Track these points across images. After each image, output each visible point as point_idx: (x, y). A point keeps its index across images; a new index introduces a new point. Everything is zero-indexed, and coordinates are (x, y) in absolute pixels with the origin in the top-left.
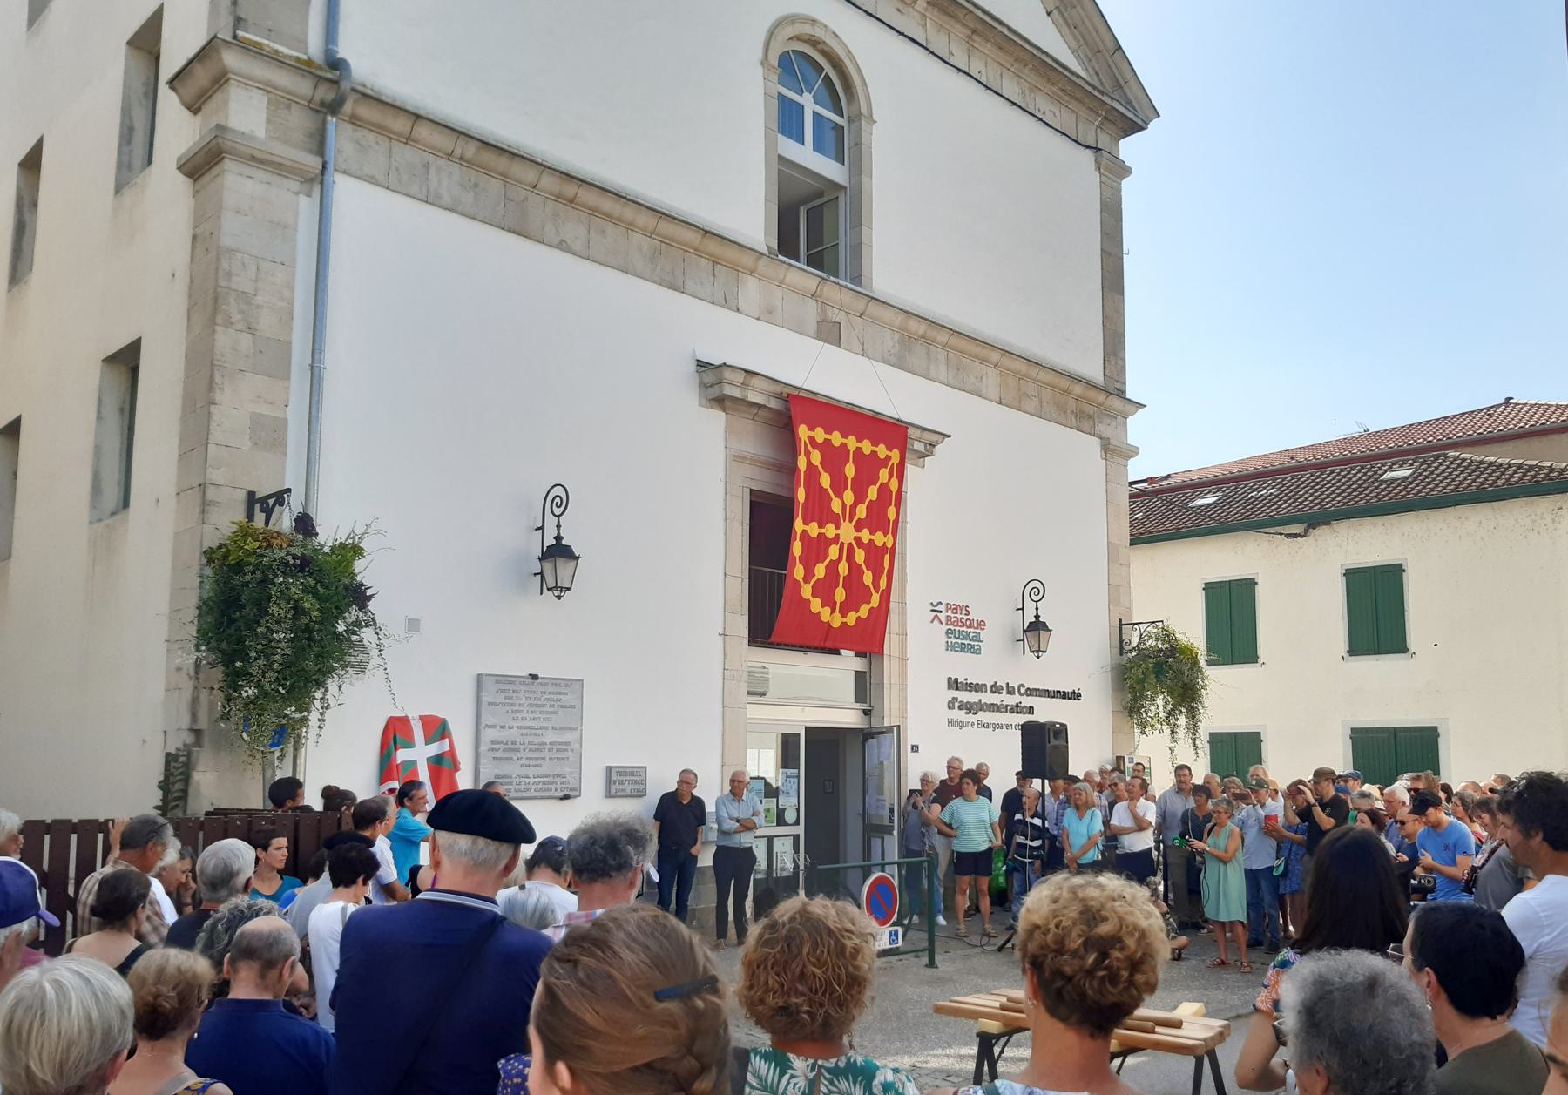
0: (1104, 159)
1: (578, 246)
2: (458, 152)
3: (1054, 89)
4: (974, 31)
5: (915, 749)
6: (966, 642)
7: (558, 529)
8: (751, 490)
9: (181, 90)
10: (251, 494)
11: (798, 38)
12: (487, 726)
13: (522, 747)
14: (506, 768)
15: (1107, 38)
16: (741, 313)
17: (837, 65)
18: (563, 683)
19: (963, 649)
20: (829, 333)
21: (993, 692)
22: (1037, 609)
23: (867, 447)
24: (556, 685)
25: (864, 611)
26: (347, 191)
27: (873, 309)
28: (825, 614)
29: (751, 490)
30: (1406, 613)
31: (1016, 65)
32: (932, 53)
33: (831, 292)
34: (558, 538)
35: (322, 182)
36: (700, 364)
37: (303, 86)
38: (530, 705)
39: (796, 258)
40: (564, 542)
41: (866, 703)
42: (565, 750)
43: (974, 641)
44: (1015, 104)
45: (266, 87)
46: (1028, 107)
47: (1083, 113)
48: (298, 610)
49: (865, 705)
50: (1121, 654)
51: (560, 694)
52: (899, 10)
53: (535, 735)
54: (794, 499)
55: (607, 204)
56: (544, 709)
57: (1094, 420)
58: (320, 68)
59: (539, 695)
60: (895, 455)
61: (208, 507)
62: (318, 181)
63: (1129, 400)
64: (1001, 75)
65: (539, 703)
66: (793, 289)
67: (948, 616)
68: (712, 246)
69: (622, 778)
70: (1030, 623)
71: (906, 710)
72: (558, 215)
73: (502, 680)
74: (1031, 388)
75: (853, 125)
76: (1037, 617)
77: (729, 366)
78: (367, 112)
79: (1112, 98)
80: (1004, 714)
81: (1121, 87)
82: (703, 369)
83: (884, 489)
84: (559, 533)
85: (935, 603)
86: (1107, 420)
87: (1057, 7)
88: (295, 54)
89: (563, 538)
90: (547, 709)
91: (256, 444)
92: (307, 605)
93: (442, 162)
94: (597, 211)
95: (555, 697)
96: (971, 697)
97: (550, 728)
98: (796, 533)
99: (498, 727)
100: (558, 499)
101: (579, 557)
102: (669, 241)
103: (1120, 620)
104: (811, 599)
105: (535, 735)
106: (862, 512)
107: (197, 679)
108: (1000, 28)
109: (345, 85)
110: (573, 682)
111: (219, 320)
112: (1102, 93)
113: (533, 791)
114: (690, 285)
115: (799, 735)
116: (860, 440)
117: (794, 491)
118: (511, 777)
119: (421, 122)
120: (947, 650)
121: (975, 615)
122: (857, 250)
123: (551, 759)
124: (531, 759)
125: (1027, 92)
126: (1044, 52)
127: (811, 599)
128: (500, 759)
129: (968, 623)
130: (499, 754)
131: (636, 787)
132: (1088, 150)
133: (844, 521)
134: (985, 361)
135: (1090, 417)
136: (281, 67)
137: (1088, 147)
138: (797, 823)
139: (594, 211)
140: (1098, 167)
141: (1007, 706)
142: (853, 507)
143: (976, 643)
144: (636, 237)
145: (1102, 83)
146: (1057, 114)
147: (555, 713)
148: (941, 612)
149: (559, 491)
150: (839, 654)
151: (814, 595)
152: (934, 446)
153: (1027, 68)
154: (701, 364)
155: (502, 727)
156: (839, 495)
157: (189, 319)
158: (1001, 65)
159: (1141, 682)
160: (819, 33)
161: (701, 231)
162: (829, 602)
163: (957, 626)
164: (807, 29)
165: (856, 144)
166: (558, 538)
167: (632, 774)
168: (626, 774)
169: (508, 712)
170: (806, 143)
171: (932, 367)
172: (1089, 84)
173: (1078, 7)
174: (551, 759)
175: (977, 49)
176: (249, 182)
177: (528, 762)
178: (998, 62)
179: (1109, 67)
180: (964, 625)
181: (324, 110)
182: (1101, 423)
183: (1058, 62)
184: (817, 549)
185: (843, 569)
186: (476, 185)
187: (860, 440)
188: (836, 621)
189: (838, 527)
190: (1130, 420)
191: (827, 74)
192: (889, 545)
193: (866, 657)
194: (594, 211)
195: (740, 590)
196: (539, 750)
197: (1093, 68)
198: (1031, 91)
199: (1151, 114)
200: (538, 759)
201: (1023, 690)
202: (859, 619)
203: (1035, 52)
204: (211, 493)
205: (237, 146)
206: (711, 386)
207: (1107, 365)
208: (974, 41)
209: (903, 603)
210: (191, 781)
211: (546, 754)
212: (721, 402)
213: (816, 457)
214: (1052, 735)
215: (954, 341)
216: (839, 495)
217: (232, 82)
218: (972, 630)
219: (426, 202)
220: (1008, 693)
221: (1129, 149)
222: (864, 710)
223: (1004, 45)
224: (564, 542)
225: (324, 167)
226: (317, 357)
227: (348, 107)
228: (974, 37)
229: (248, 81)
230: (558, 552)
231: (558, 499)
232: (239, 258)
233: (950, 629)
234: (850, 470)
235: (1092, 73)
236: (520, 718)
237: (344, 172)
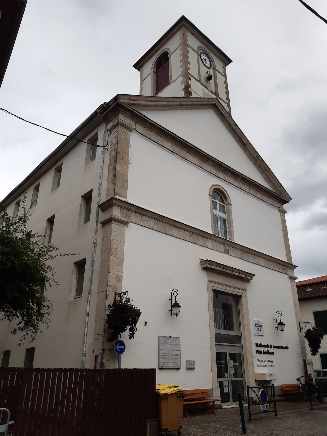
10: (116, 293)
34: (176, 302)
44: (260, 199)
46: (274, 205)
52: (234, 181)
73: (163, 337)
76: (281, 321)
82: (201, 261)
84: (176, 301)
87: (267, 178)
89: (177, 302)
95: (175, 342)
100: (175, 292)
103: (299, 322)
107: (104, 337)
115: (226, 353)
124: (170, 358)
130: (164, 357)
137: (277, 207)
138: (228, 377)
145: (278, 193)
146: (269, 200)
157: (102, 254)
166: (176, 302)
174: (174, 358)
182: (288, 271)
197: (276, 190)
204: (108, 293)
231: (175, 292)
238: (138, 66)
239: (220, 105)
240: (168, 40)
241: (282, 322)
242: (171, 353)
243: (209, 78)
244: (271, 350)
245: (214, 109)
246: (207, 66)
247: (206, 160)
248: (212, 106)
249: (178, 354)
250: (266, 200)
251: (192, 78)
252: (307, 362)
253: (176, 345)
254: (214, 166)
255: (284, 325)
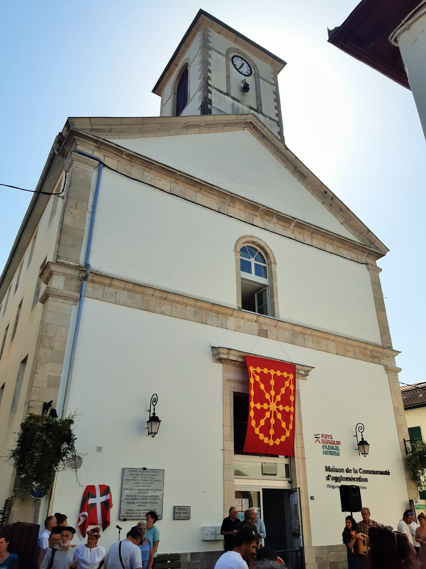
0: (370, 267)
1: (167, 313)
2: (127, 287)
3: (346, 246)
4: (312, 232)
5: (312, 498)
6: (332, 451)
7: (154, 411)
8: (234, 392)
9: (43, 278)
11: (248, 242)
12: (125, 489)
13: (138, 498)
14: (132, 507)
15: (364, 228)
16: (228, 329)
17: (262, 248)
18: (156, 471)
19: (331, 453)
20: (263, 333)
21: (347, 472)
22: (362, 435)
23: (279, 373)
24: (153, 472)
25: (283, 438)
26: (88, 303)
27: (279, 324)
28: (266, 440)
29: (234, 392)
30: (418, 408)
31: (330, 241)
32: (297, 241)
33: (263, 319)
35: (80, 300)
36: (213, 348)
37: (76, 273)
38: (143, 480)
39: (254, 311)
40: (156, 415)
41: (289, 478)
42: (157, 499)
43: (336, 450)
44: (331, 253)
45: (64, 274)
47: (359, 253)
48: (45, 445)
49: (289, 479)
50: (407, 454)
51: (155, 475)
52: (284, 230)
53: (144, 492)
54: (249, 394)
55: (178, 298)
56: (148, 482)
57: (379, 358)
58: (83, 267)
59: (146, 476)
60: (291, 376)
61: (30, 409)
62: (79, 300)
63: (394, 350)
64: (325, 244)
65: (146, 479)
66: (248, 320)
67: (323, 440)
68: (216, 308)
69: (180, 511)
70: (360, 441)
71: (307, 481)
72: (161, 303)
74: (350, 348)
75: (269, 266)
76: (363, 439)
77: (221, 347)
78: (96, 278)
79: (369, 247)
80: (353, 482)
81: (373, 243)
82: (213, 349)
83: (288, 389)
84: (154, 412)
85: (316, 434)
86: (385, 358)
88: (75, 264)
90: (149, 482)
91: (49, 386)
92: (48, 443)
93: (121, 291)
94: (174, 301)
95: (153, 477)
96: (338, 475)
97: (150, 490)
98: (251, 408)
99: (129, 489)
101: (161, 421)
102: (201, 308)
103: (404, 439)
104: (259, 434)
105: (144, 492)
106: (279, 398)
108: (322, 230)
109: (88, 271)
110: (161, 471)
111: (41, 346)
112: (365, 246)
113: (142, 516)
114: (208, 322)
116: (275, 371)
117: (249, 390)
118: (133, 510)
119: (113, 279)
120: (324, 454)
121: (335, 439)
122: (273, 304)
123: (150, 503)
124: (142, 503)
125: (336, 249)
126: (340, 236)
127: (259, 434)
128: (130, 503)
129: (332, 442)
131: (186, 515)
132: (363, 264)
133: (271, 402)
134: (328, 339)
135: (377, 357)
136: (69, 269)
139: (173, 301)
140: (368, 269)
141: (355, 478)
142: (275, 397)
143: (337, 451)
144: (189, 308)
145: (365, 243)
146: (349, 254)
147: (153, 483)
148: (319, 438)
149: (155, 396)
150: (278, 457)
151: (260, 432)
152: (308, 372)
153: (335, 241)
154: (213, 348)
155: (131, 489)
156: (269, 392)
158: (324, 241)
159: (415, 466)
160: (255, 240)
161: (212, 304)
162: (267, 435)
163: (327, 443)
164: (251, 239)
165: (271, 272)
166: (154, 414)
167: (184, 509)
168: (182, 509)
169: (133, 483)
170: (252, 273)
171: (306, 343)
172: (361, 244)
173: (352, 220)
174: (150, 503)
175: (314, 238)
176: (57, 303)
177: (141, 504)
178: (323, 241)
179: (367, 237)
180: (330, 443)
181: (83, 279)
183: (346, 238)
184: (260, 414)
185: (272, 421)
186: (133, 297)
187: (275, 371)
188: (271, 443)
189: (269, 404)
190: (396, 358)
191: (259, 252)
192: (292, 411)
193: (288, 458)
194: (173, 301)
195: (230, 431)
196: (146, 499)
198: (337, 248)
199: (387, 250)
200: (145, 503)
201: (361, 471)
202: (281, 442)
203: (336, 236)
205: (53, 293)
206: (216, 355)
207: (382, 338)
208: (313, 235)
209: (302, 435)
210: (11, 510)
211: (148, 501)
212: (220, 360)
213: (258, 378)
214: (352, 491)
215: (314, 333)
216: (269, 392)
217: (54, 274)
218: (334, 445)
219: (115, 304)
220: (355, 472)
221: (380, 262)
222: (288, 481)
223: (325, 235)
224: (156, 415)
225: (81, 296)
226: (72, 355)
227: (90, 277)
228: (313, 234)
229: (59, 273)
230: (154, 419)
232: (50, 326)
233: (324, 445)
234: (272, 382)
235: (361, 240)
236: (138, 486)
237: (88, 297)
238: (157, 90)
239: (259, 123)
240: (188, 46)
241: (364, 440)
242: (145, 495)
243: (246, 88)
244: (364, 476)
245: (251, 130)
246: (245, 74)
247: (231, 201)
248: (246, 126)
249: (157, 496)
250: (344, 254)
251: (214, 91)
252: (416, 504)
253: (156, 481)
254: (245, 210)
255: (369, 445)
